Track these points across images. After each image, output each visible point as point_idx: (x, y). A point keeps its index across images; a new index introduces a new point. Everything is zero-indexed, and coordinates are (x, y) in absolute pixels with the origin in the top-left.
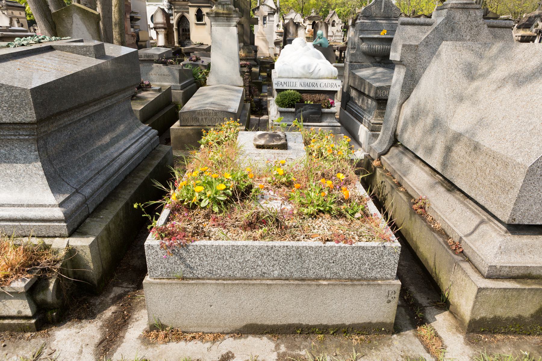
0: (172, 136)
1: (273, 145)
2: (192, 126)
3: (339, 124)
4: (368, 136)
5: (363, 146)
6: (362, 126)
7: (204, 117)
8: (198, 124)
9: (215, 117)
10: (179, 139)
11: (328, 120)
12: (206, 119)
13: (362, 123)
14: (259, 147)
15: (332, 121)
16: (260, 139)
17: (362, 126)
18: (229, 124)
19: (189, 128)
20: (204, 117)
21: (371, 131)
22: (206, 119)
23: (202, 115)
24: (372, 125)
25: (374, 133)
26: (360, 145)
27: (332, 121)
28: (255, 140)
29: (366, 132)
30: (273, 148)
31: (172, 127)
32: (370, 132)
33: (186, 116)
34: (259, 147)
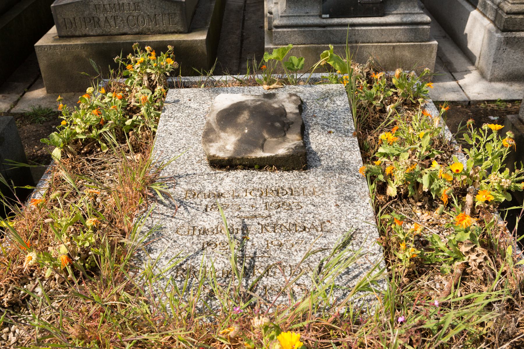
0: (43, 64)
1: (261, 159)
2: (85, 36)
3: (428, 19)
4: (495, 43)
5: (481, 62)
6: (475, 14)
7: (109, 15)
8: (99, 31)
9: (135, 13)
10: (58, 67)
11: (401, 10)
12: (115, 18)
13: (475, 7)
14: (217, 164)
15: (409, 10)
16: (223, 128)
17: (475, 14)
18: (143, 63)
19: (79, 42)
20: (109, 15)
21: (503, 31)
22: (115, 18)
23: (105, 10)
24: (505, 16)
25: (510, 35)
26: (470, 58)
27: (409, 10)
28: (208, 136)
29: (489, 32)
30: (260, 168)
31: (37, 44)
32: (499, 35)
33: (70, 15)
34: (217, 164)
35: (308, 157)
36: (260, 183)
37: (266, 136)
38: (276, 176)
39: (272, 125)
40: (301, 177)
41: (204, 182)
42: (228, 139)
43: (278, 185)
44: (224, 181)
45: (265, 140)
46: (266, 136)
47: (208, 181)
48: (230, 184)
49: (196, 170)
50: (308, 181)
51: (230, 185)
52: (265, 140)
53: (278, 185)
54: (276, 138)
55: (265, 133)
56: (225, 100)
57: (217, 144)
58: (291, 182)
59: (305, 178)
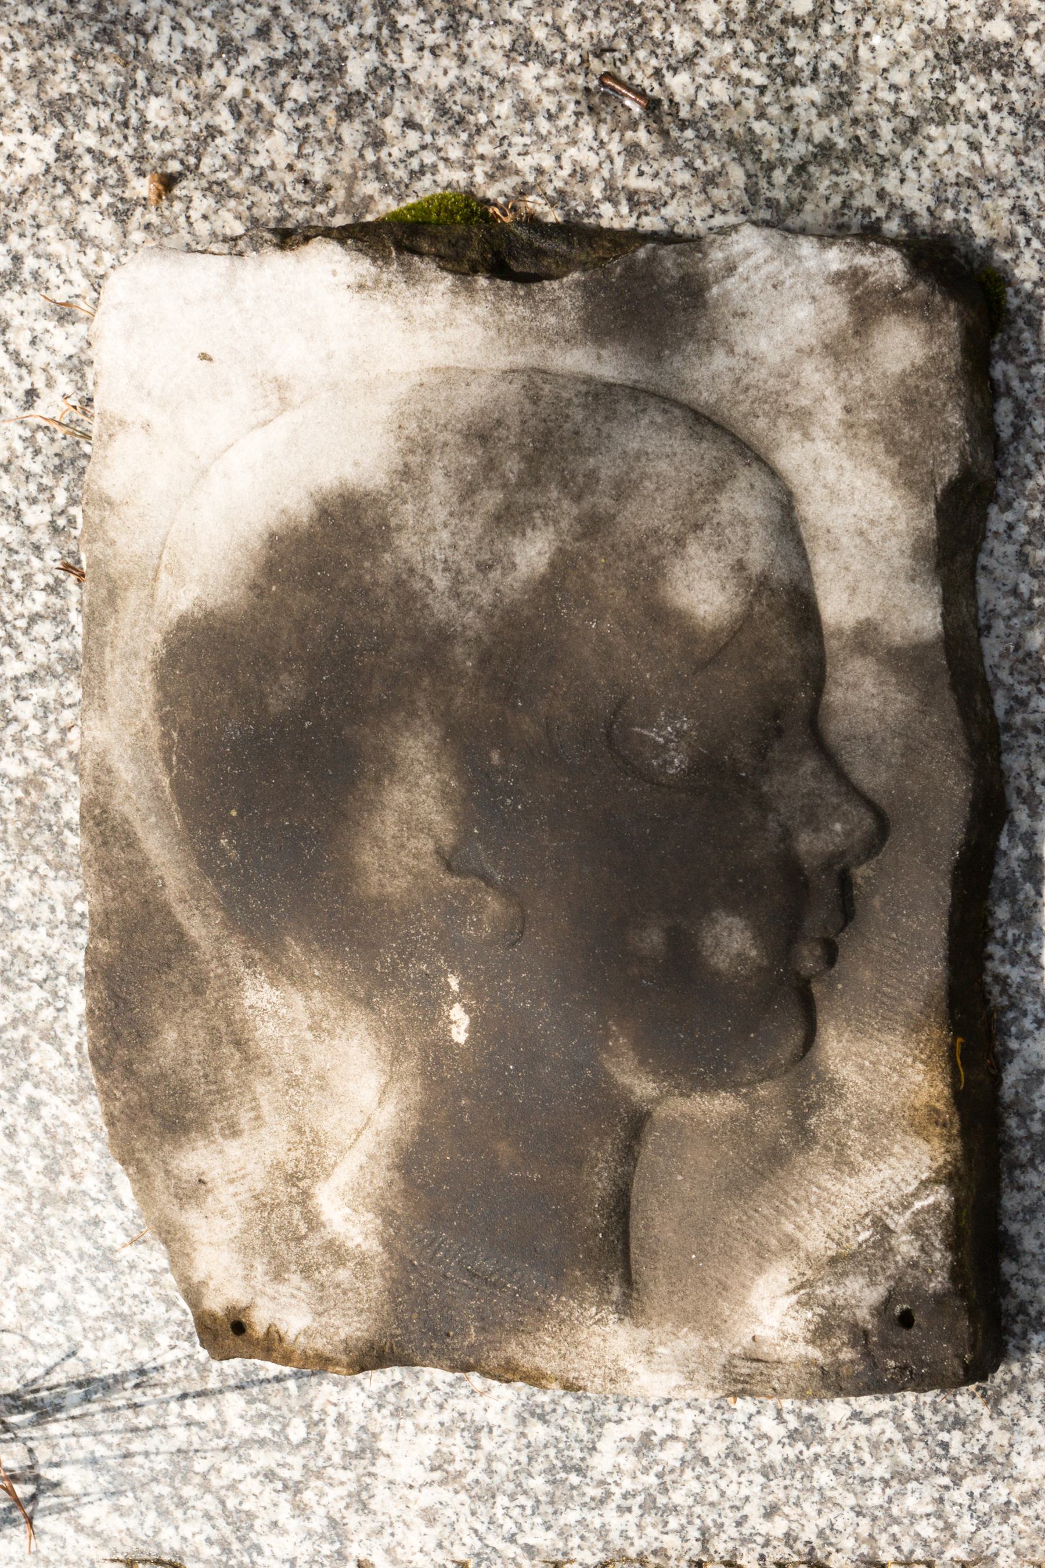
35: (1011, 1201)
36: (649, 1505)
37: (643, 1087)
38: (767, 1423)
39: (683, 961)
40: (955, 1438)
41: (233, 1470)
42: (322, 1082)
43: (778, 1527)
44: (381, 1467)
45: (637, 1124)
46: (643, 1087)
47: (263, 1459)
48: (427, 1498)
49: (148, 1332)
50: (1001, 1492)
51: (430, 1517)
52: (637, 1124)
53: (778, 1527)
54: (734, 1087)
55: (630, 1060)
56: (126, 772)
57: (233, 1148)
58: (875, 1497)
59: (983, 1459)
